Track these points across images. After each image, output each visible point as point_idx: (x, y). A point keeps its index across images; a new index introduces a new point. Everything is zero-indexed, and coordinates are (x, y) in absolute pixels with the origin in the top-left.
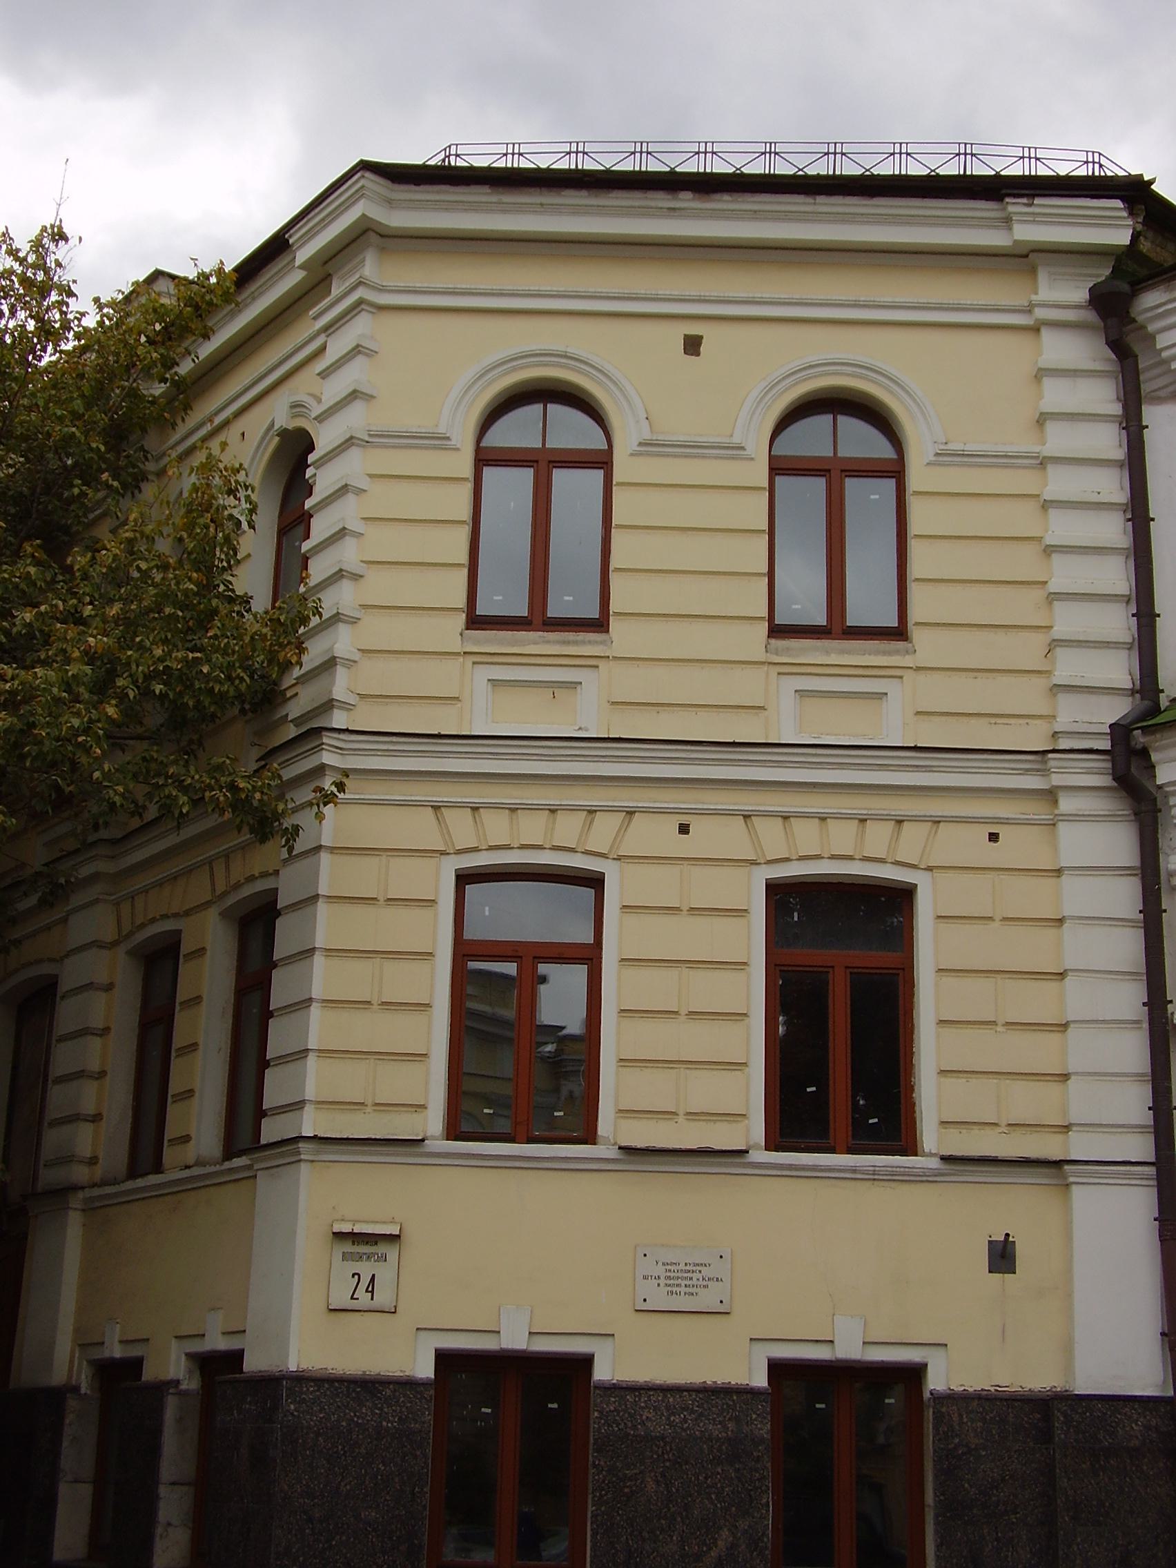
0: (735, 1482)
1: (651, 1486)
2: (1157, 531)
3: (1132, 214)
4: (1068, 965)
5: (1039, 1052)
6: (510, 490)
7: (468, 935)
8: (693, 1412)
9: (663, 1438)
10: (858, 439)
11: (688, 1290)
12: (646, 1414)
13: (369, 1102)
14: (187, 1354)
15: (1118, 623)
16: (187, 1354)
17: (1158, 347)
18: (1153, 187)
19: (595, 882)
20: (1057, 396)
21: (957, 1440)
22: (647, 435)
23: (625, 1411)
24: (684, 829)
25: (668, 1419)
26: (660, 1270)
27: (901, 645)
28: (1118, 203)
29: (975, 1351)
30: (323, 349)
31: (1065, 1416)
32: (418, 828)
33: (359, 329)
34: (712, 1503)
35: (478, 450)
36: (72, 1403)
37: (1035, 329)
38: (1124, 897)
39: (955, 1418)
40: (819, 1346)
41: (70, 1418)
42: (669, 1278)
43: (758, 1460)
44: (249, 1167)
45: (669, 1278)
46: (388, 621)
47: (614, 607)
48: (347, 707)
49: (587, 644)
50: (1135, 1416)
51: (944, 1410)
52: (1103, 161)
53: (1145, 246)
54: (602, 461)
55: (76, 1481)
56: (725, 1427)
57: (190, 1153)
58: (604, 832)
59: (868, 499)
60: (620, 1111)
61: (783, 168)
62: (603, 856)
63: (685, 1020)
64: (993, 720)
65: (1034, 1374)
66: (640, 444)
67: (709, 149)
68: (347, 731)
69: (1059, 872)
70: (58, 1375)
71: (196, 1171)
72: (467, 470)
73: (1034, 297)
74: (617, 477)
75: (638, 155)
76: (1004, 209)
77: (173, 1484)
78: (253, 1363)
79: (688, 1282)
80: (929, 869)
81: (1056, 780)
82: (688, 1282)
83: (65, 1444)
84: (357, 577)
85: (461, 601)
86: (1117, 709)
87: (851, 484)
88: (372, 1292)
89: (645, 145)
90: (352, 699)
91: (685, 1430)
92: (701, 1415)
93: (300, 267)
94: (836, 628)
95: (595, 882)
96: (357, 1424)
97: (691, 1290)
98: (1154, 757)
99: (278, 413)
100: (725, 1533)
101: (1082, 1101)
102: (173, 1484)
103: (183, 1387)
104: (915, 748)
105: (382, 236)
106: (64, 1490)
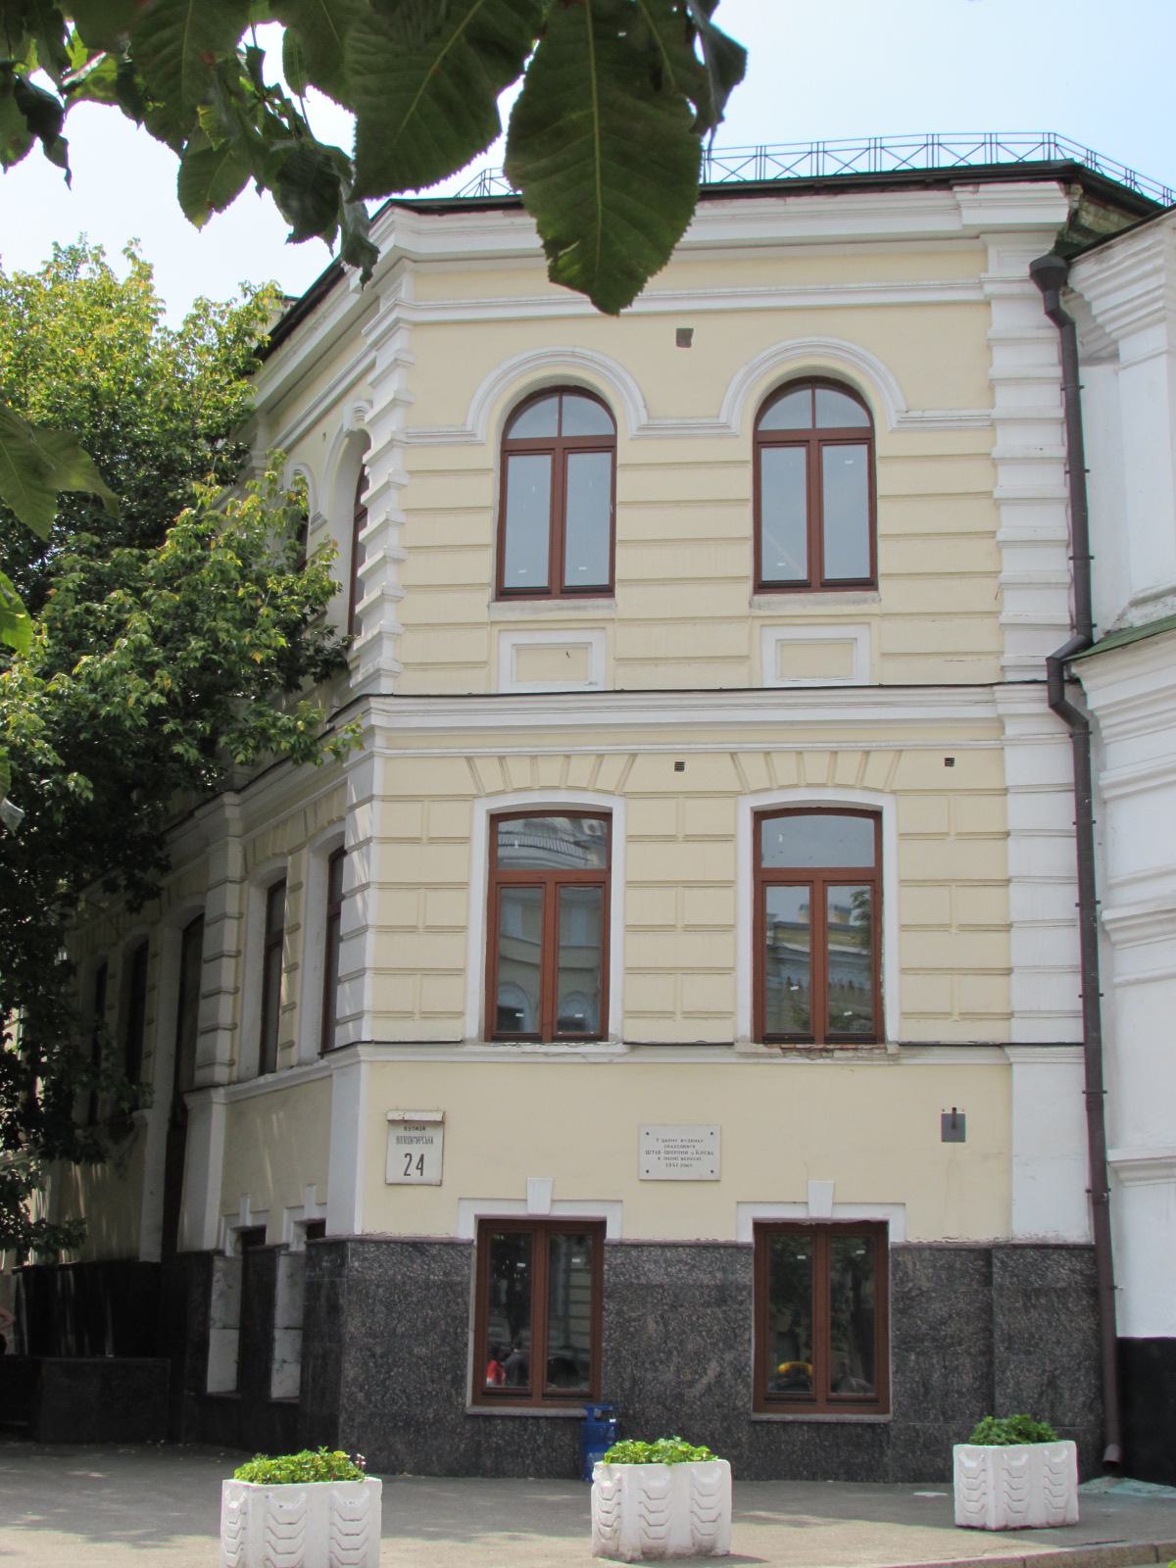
0: (723, 1322)
1: (651, 1325)
2: (1091, 481)
3: (1068, 193)
4: (1012, 873)
5: (985, 950)
6: (787, 464)
7: (766, 864)
8: (686, 1264)
9: (661, 1286)
10: (835, 411)
11: (684, 1162)
12: (647, 1266)
13: (416, 1010)
14: (295, 1223)
15: (1059, 565)
16: (295, 1223)
17: (1094, 312)
18: (290, 229)
19: (876, 815)
20: (1005, 361)
21: (910, 1285)
22: (644, 421)
23: (630, 1263)
24: (679, 767)
25: (666, 1269)
26: (660, 1146)
27: (870, 594)
28: (1054, 185)
29: (930, 1209)
30: (372, 366)
31: (1002, 1262)
32: (454, 777)
33: (398, 342)
34: (703, 1339)
35: (756, 433)
36: (218, 1264)
37: (987, 303)
38: (1062, 810)
39: (910, 1265)
40: (796, 1207)
41: (217, 1276)
42: (668, 1153)
43: (741, 1303)
44: (326, 1068)
45: (668, 1153)
46: (419, 598)
47: (618, 576)
48: (394, 675)
49: (595, 607)
50: (1062, 1262)
51: (900, 1259)
52: (1059, 141)
53: (1087, 219)
54: (865, 438)
55: (224, 1328)
56: (714, 1277)
57: (294, 1055)
58: (878, 770)
59: (842, 464)
60: (627, 1012)
61: (1005, 158)
62: (611, 793)
63: (680, 937)
64: (949, 658)
65: (982, 1231)
66: (639, 429)
67: (936, 141)
68: (392, 695)
69: (1005, 791)
70: (208, 1243)
71: (296, 1070)
72: (747, 453)
73: (982, 275)
74: (880, 450)
75: (872, 151)
76: (954, 197)
77: (287, 1328)
78: (331, 1231)
79: (683, 1156)
80: (894, 792)
81: (1001, 709)
82: (683, 1156)
83: (214, 1297)
84: (399, 561)
85: (747, 569)
86: (1058, 642)
87: (828, 452)
88: (422, 1169)
89: (878, 141)
90: (397, 668)
91: (679, 1279)
92: (694, 1266)
93: (353, 291)
94: (816, 583)
95: (876, 815)
96: (410, 1278)
97: (686, 1162)
98: (1086, 685)
99: (345, 418)
100: (714, 1364)
101: (1022, 993)
102: (287, 1328)
103: (293, 1249)
104: (881, 686)
105: (415, 261)
106: (215, 1336)
